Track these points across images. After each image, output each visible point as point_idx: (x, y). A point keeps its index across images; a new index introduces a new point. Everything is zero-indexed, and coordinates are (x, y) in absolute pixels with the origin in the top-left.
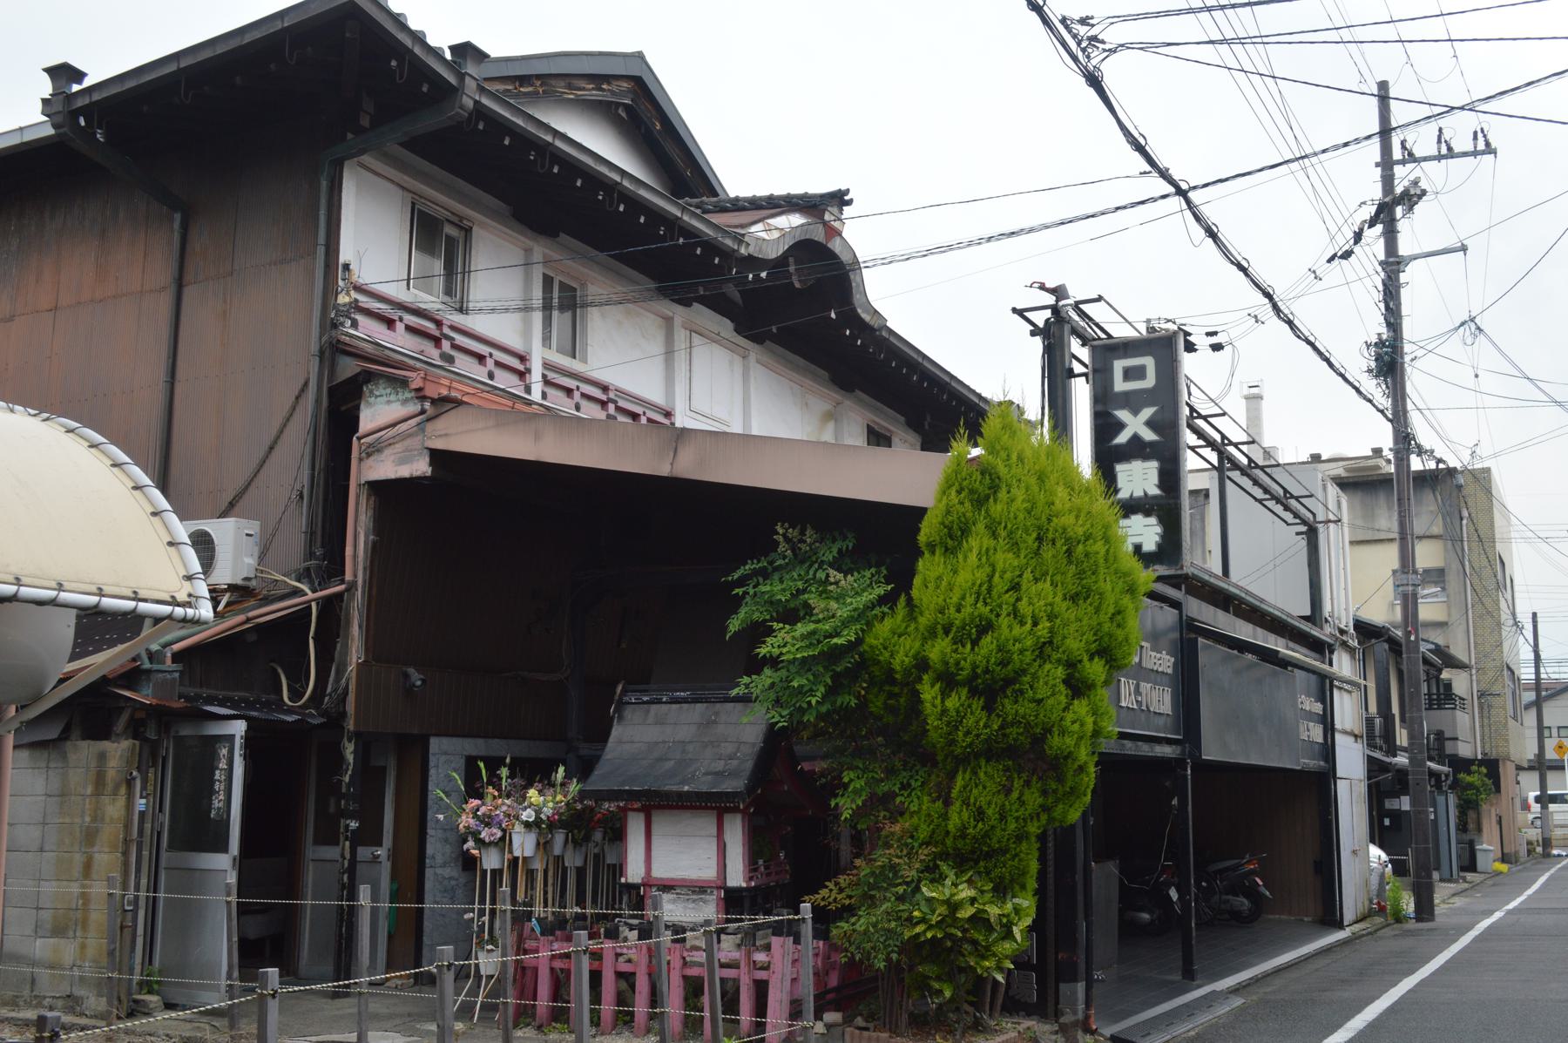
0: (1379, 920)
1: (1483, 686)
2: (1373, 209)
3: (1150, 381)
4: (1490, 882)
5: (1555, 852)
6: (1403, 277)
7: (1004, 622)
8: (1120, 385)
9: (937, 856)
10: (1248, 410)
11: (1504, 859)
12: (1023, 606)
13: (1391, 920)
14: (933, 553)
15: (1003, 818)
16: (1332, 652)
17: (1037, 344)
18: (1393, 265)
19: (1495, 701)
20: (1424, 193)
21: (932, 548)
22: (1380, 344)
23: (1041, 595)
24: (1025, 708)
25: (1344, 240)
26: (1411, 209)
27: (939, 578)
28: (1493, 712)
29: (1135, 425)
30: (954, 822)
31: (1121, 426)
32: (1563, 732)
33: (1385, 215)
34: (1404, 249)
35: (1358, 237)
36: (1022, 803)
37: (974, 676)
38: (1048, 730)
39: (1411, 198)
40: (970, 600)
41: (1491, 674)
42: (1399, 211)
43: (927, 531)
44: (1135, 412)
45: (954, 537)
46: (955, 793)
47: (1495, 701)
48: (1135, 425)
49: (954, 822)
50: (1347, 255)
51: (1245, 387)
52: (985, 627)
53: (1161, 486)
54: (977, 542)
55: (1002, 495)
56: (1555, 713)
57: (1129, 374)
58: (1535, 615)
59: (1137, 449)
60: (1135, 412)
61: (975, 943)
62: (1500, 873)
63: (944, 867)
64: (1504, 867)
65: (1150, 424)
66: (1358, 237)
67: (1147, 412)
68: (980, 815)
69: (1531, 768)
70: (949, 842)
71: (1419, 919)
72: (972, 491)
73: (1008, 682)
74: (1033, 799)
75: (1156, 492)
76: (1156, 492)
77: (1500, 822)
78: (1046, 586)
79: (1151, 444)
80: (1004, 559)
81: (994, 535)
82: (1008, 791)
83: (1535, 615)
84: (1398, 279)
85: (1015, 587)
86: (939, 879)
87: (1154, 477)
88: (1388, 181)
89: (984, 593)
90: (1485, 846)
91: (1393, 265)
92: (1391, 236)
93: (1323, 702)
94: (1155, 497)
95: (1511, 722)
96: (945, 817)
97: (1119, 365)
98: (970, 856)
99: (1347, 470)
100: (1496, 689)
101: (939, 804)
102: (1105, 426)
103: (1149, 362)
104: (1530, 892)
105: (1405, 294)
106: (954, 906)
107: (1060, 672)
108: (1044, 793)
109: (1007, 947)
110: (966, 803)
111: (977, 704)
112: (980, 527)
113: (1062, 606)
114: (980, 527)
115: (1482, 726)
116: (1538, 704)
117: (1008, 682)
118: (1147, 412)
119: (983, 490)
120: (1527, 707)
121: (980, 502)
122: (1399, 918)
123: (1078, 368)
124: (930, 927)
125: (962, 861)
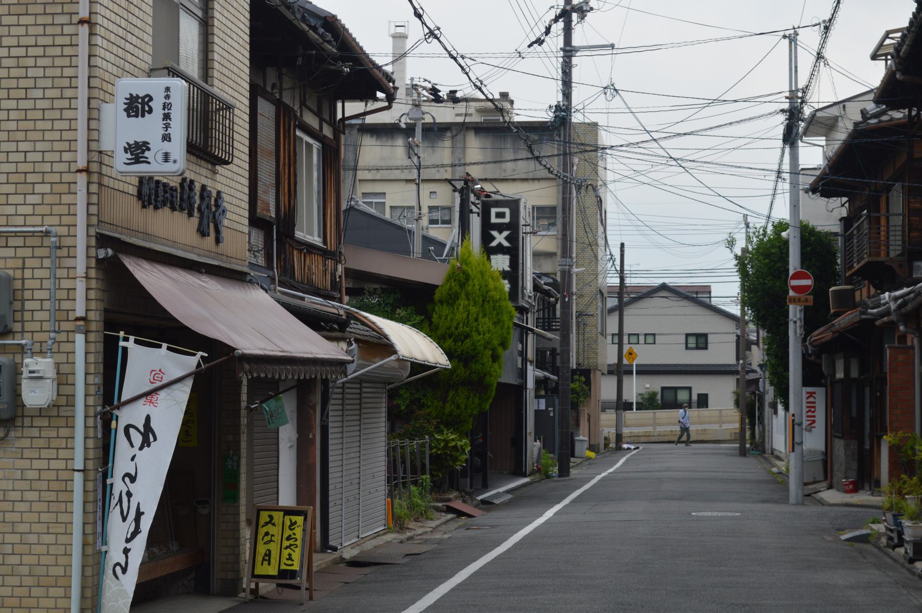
0: (538, 476)
1: (581, 308)
2: (559, 11)
4: (586, 463)
5: (625, 446)
7: (474, 334)
8: (494, 220)
9: (439, 423)
11: (591, 448)
12: (481, 329)
13: (543, 477)
14: (442, 304)
15: (466, 408)
16: (527, 313)
18: (569, 51)
20: (592, 9)
21: (441, 302)
22: (558, 107)
23: (486, 323)
24: (479, 367)
25: (539, 32)
26: (583, 18)
27: (447, 316)
28: (588, 329)
29: (500, 238)
30: (448, 409)
31: (493, 238)
34: (576, 41)
35: (548, 31)
36: (473, 403)
37: (462, 354)
38: (485, 375)
40: (461, 325)
41: (587, 299)
42: (575, 16)
43: (437, 296)
44: (500, 232)
45: (452, 299)
46: (449, 398)
48: (500, 238)
49: (448, 409)
50: (540, 42)
51: (393, 25)
52: (467, 336)
53: (510, 267)
54: (463, 302)
55: (470, 282)
57: (499, 215)
58: (622, 245)
59: (500, 249)
60: (500, 232)
61: (451, 456)
62: (590, 458)
63: (442, 427)
64: (592, 455)
65: (507, 238)
66: (548, 31)
67: (506, 233)
68: (458, 407)
69: (610, 373)
70: (444, 418)
71: (560, 476)
72: (459, 281)
73: (474, 357)
74: (477, 401)
75: (508, 269)
76: (508, 269)
77: (589, 420)
78: (486, 319)
79: (507, 248)
80: (473, 310)
81: (468, 300)
82: (468, 398)
83: (622, 245)
84: (570, 61)
85: (476, 320)
86: (441, 432)
87: (507, 262)
89: (467, 323)
90: (581, 438)
92: (568, 32)
93: (522, 343)
94: (507, 272)
95: (600, 336)
96: (443, 408)
97: (493, 211)
98: (452, 423)
99: (480, 111)
100: (591, 310)
101: (441, 403)
102: (486, 238)
103: (507, 211)
104: (611, 470)
106: (447, 442)
107: (490, 352)
108: (480, 399)
109: (464, 457)
110: (453, 402)
111: (461, 364)
112: (463, 295)
113: (492, 327)
114: (463, 295)
115: (578, 341)
116: (620, 309)
117: (474, 357)
118: (506, 233)
119: (463, 281)
120: (611, 311)
121: (462, 285)
122: (548, 477)
123: (474, 209)
124: (439, 449)
125: (448, 425)
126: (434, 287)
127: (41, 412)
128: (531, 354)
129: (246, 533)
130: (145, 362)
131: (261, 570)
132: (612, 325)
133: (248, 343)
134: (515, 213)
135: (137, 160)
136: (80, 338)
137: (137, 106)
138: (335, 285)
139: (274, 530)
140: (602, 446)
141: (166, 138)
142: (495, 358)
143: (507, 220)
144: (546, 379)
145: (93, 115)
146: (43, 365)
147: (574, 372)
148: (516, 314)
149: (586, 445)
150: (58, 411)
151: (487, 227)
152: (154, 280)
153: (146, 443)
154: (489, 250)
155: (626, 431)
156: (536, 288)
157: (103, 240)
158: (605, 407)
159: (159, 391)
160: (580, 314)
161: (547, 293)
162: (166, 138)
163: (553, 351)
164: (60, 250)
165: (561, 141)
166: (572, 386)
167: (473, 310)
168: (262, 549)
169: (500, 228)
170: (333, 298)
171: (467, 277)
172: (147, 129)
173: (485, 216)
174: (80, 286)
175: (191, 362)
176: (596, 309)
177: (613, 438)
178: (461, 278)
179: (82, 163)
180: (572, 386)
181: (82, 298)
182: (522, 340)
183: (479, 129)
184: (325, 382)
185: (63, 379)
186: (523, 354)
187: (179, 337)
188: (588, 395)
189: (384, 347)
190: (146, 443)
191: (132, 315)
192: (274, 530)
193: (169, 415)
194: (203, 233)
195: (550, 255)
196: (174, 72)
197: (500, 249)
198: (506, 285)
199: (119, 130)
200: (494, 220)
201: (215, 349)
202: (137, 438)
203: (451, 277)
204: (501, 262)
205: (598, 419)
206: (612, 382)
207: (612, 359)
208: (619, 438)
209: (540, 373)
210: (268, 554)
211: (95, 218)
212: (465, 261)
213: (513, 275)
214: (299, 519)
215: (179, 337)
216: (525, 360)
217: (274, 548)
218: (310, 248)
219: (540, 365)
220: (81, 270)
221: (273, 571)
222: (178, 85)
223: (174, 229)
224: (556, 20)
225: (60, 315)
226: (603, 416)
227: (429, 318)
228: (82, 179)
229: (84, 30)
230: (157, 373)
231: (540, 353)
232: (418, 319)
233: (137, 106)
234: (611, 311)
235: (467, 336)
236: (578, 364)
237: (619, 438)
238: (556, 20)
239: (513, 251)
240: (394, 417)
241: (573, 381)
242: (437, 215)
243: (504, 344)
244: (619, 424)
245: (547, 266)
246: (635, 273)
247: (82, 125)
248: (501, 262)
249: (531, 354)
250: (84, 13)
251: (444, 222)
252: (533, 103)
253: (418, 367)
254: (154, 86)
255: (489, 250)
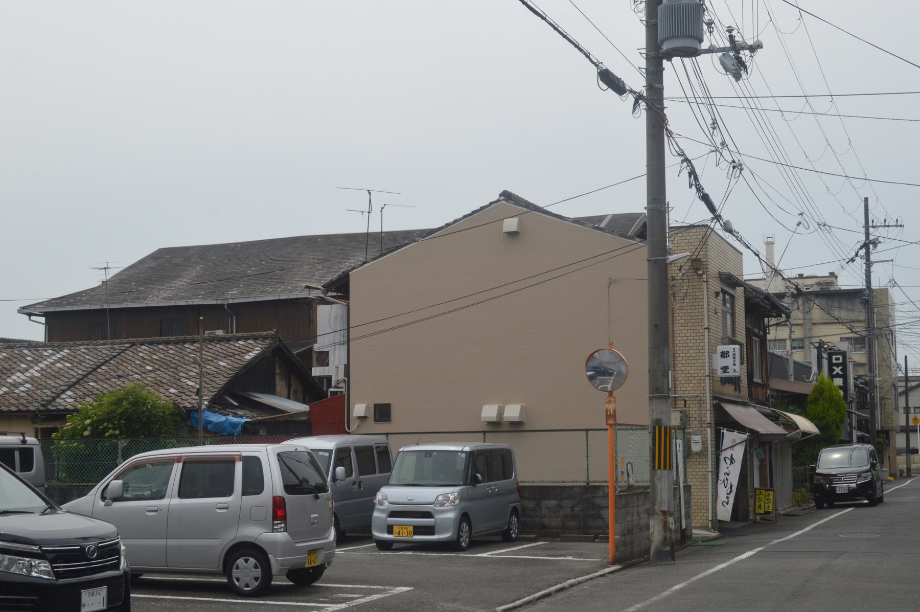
3: (841, 361)
6: (872, 269)
8: (834, 361)
10: (767, 250)
11: (891, 475)
17: (816, 350)
19: (888, 402)
29: (838, 370)
32: (917, 410)
33: (866, 246)
39: (875, 243)
42: (871, 246)
43: (809, 399)
45: (816, 401)
47: (888, 402)
48: (838, 370)
50: (852, 260)
52: (824, 418)
54: (821, 402)
56: (917, 399)
57: (837, 359)
58: (906, 357)
59: (838, 375)
64: (892, 479)
66: (857, 255)
69: (902, 431)
80: (826, 405)
83: (906, 357)
88: (867, 234)
91: (869, 264)
92: (868, 254)
93: (173, 463)
97: (834, 357)
99: (819, 284)
100: (888, 396)
102: (831, 370)
103: (840, 357)
105: (872, 275)
116: (906, 393)
120: (901, 394)
121: (821, 394)
126: (806, 396)
127: (697, 453)
128: (854, 424)
129: (751, 501)
130: (730, 437)
131: (757, 511)
132: (902, 402)
133: (762, 431)
134: (844, 358)
135: (725, 372)
136: (709, 429)
137: (724, 355)
138: (767, 399)
139: (762, 497)
140: (898, 475)
141: (734, 365)
142: (838, 428)
143: (841, 361)
144: (863, 436)
145: (710, 358)
146: (698, 438)
147: (879, 432)
148: (846, 405)
149: (888, 474)
150: (703, 453)
151: (831, 365)
152: (730, 409)
153: (732, 463)
154: (832, 376)
155: (913, 466)
156: (856, 386)
157: (715, 398)
158: (899, 453)
159: (734, 446)
160: (881, 399)
161: (862, 388)
162: (734, 365)
163: (867, 420)
164: (701, 402)
165: (867, 300)
166: (878, 440)
167: (826, 405)
168: (757, 504)
169: (838, 365)
170: (765, 405)
171: (823, 390)
172: (728, 362)
173: (830, 359)
174: (708, 413)
175: (745, 436)
176: (891, 395)
177: (905, 470)
178: (820, 390)
179: (707, 374)
180: (878, 440)
181: (709, 417)
182: (850, 417)
183: (817, 295)
184: (770, 442)
185: (704, 443)
186: (850, 424)
187: (741, 428)
188: (888, 445)
189: (795, 426)
190: (732, 463)
191: (723, 421)
192: (762, 497)
193: (739, 453)
194: (736, 390)
195: (862, 365)
196: (734, 342)
197: (838, 375)
198: (841, 393)
199: (720, 362)
200: (834, 361)
201: (753, 432)
202: (729, 462)
203: (815, 390)
204: (838, 382)
205: (895, 459)
206: (904, 436)
207: (903, 423)
208: (909, 469)
209: (859, 433)
210: (760, 506)
211: (713, 391)
212: (822, 383)
213: (845, 387)
214: (771, 493)
215: (741, 428)
216: (851, 427)
217: (762, 503)
218: (758, 384)
219: (860, 428)
220: (708, 408)
221: (762, 511)
222: (737, 347)
223: (729, 389)
224: (861, 248)
225: (701, 422)
226: (898, 458)
227: (805, 409)
228: (707, 378)
229: (706, 331)
230: (734, 440)
231: (859, 422)
232: (800, 410)
233: (724, 355)
234: (901, 394)
235: (824, 418)
236: (882, 427)
237: (909, 469)
238: (861, 248)
239: (844, 376)
240: (795, 457)
241: (878, 437)
242: (796, 344)
243: (842, 421)
244: (908, 462)
245: (862, 371)
246: (914, 370)
247: (707, 361)
248: (838, 382)
249: (854, 424)
250: (706, 326)
251: (799, 348)
252: (850, 279)
253: (805, 434)
254: (729, 348)
255: (832, 376)
